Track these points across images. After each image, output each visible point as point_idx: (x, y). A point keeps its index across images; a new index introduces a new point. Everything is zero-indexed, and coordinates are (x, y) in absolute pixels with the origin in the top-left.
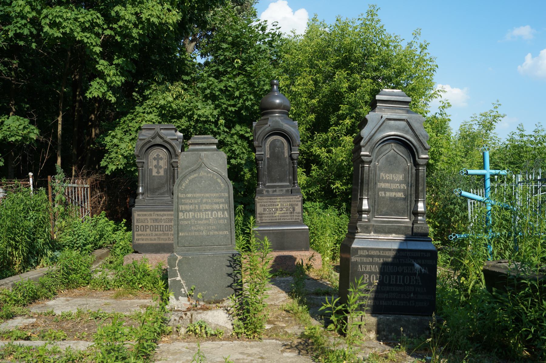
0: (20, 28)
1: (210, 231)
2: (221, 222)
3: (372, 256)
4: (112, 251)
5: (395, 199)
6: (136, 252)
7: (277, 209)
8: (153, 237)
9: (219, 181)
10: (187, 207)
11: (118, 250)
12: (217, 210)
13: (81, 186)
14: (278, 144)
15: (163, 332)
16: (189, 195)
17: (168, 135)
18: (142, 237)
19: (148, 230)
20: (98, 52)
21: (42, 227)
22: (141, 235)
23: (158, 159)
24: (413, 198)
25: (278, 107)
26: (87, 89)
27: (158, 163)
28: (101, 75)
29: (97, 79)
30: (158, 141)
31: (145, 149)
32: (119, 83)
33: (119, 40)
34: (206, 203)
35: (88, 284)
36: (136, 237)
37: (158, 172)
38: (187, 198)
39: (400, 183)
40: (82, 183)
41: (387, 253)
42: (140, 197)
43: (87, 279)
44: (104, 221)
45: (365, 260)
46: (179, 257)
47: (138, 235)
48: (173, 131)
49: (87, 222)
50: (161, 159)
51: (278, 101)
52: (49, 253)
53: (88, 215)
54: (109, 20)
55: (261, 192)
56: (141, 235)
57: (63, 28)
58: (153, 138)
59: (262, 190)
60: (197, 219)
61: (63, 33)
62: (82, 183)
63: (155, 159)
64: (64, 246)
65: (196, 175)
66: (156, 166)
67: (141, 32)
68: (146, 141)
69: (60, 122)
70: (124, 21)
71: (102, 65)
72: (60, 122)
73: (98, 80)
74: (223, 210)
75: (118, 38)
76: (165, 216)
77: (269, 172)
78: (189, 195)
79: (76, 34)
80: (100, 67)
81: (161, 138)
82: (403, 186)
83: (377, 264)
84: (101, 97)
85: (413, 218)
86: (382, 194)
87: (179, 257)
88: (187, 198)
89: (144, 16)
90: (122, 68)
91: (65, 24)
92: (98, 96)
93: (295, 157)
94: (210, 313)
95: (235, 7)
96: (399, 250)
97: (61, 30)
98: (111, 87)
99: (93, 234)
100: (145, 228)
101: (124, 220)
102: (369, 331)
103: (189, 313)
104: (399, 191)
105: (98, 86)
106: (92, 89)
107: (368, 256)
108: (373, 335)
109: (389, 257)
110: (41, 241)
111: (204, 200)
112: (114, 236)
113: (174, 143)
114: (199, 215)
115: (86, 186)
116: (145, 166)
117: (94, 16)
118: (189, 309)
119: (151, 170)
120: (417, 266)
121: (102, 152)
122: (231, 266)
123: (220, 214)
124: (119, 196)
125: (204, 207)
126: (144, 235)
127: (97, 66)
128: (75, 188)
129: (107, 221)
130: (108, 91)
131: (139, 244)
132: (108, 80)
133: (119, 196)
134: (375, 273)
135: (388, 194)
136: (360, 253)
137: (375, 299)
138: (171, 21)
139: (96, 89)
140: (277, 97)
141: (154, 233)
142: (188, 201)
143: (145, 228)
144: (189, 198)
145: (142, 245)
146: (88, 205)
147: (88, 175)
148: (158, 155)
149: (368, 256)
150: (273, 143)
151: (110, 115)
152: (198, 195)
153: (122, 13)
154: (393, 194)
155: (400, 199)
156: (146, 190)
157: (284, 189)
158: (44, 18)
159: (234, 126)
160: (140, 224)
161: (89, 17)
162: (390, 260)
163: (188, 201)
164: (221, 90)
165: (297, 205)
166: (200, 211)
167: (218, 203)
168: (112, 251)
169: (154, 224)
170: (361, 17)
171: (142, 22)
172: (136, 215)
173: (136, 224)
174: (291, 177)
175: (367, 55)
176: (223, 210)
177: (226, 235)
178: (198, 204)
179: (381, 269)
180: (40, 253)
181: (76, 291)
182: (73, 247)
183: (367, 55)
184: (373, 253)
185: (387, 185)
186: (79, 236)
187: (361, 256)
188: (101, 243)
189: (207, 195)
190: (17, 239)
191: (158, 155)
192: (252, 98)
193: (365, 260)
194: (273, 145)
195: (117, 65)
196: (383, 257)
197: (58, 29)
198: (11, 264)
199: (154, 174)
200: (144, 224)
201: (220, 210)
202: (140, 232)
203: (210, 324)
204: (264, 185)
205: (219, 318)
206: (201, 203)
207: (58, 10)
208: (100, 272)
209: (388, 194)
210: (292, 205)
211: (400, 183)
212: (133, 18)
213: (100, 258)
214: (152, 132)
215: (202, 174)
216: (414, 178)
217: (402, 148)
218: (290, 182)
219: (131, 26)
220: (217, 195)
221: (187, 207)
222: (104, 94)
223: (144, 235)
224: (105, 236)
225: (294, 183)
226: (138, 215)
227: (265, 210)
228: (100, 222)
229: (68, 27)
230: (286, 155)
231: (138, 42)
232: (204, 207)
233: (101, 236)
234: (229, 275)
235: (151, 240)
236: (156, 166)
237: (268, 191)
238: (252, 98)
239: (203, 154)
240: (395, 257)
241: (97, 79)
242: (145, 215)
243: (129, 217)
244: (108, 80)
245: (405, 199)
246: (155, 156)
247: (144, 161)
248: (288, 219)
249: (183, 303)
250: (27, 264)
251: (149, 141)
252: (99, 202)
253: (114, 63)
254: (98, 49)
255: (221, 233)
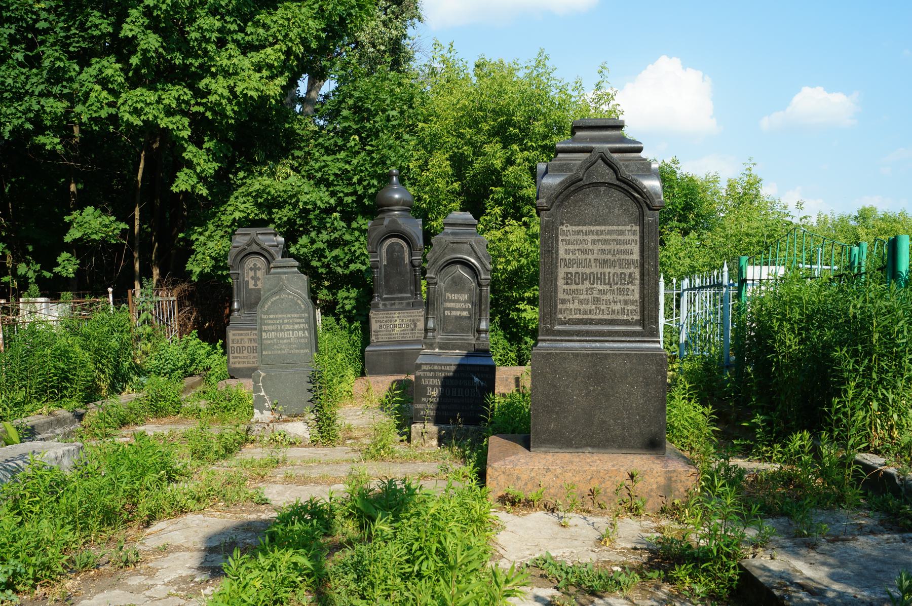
0: (95, 112)
1: (291, 349)
2: (302, 341)
3: (434, 371)
4: (206, 380)
5: (460, 317)
6: (232, 377)
7: (395, 326)
8: (251, 360)
9: (299, 302)
10: (270, 328)
11: (213, 378)
12: (298, 330)
13: (166, 299)
14: (397, 248)
15: (247, 440)
16: (272, 316)
17: (266, 241)
18: (238, 360)
19: (245, 352)
20: (186, 137)
21: (126, 349)
22: (237, 357)
23: (255, 269)
24: (477, 317)
25: (397, 203)
26: (173, 181)
27: (255, 273)
28: (190, 164)
29: (185, 169)
30: (255, 248)
31: (239, 258)
32: (211, 171)
33: (210, 117)
34: (288, 323)
35: (178, 412)
36: (231, 360)
37: (255, 285)
38: (269, 319)
39: (465, 302)
40: (167, 296)
41: (448, 368)
42: (236, 314)
43: (177, 407)
44: (195, 342)
45: (428, 374)
46: (263, 374)
47: (233, 358)
48: (272, 237)
49: (178, 345)
50: (259, 269)
51: (397, 196)
52: (135, 378)
53: (175, 336)
54: (200, 94)
55: (376, 306)
56: (237, 357)
57: (145, 114)
58: (248, 245)
59: (378, 304)
60: (279, 339)
61: (143, 121)
62: (167, 296)
63: (251, 269)
64: (149, 372)
65: (278, 297)
66: (252, 278)
67: (236, 108)
68: (240, 248)
69: (137, 217)
70: (216, 96)
71: (190, 152)
72: (137, 217)
73: (185, 170)
74: (304, 330)
75: (209, 114)
76: (253, 335)
77: (387, 281)
78: (272, 316)
79: (159, 121)
80: (187, 155)
81: (258, 245)
82: (468, 305)
83: (439, 377)
84: (190, 190)
85: (476, 334)
86: (447, 313)
87: (263, 374)
88: (269, 319)
89: (238, 90)
90: (214, 154)
91: (147, 109)
92: (187, 190)
93: (416, 263)
94: (290, 424)
95: (389, 7)
96: (459, 366)
97: (142, 117)
98: (202, 178)
99: (182, 358)
100: (241, 349)
101: (220, 341)
102: (431, 438)
103: (271, 425)
104: (464, 310)
105: (186, 178)
106: (178, 182)
107: (431, 371)
108: (435, 442)
109: (450, 371)
110: (126, 365)
111: (286, 321)
112: (207, 360)
113: (272, 250)
114: (283, 335)
115: (172, 299)
116: (241, 278)
117: (181, 92)
118: (271, 422)
119: (247, 283)
120: (476, 379)
121: (188, 250)
122: (311, 382)
123: (301, 334)
124: (211, 308)
125: (285, 327)
126: (240, 358)
127: (184, 155)
128: (159, 302)
129: (200, 343)
130: (198, 183)
131: (235, 368)
132: (198, 170)
133: (211, 308)
134: (437, 386)
135: (453, 313)
136: (423, 367)
137: (437, 410)
138: (272, 93)
139: (183, 182)
140: (396, 191)
141: (252, 355)
142: (270, 322)
143: (241, 349)
144: (272, 319)
145: (238, 370)
146: (175, 323)
147: (174, 284)
148: (255, 265)
149: (431, 371)
150: (391, 246)
151: (198, 210)
152: (279, 316)
153: (213, 87)
154: (458, 313)
155: (465, 317)
156: (242, 305)
157: (405, 302)
158: (123, 104)
159: (355, 219)
160: (235, 345)
161: (174, 94)
162: (451, 374)
163: (270, 322)
164: (336, 175)
165: (419, 320)
166: (282, 331)
167: (299, 323)
168: (206, 380)
169: (251, 345)
170: (529, 64)
171: (235, 96)
172: (231, 334)
173: (231, 345)
174: (412, 288)
175: (531, 118)
176: (304, 330)
177: (306, 354)
178: (280, 324)
179: (442, 383)
180: (125, 379)
181: (166, 420)
182: (159, 374)
183: (531, 118)
184: (435, 368)
185: (452, 305)
186: (166, 360)
187: (424, 371)
188: (192, 369)
189: (288, 316)
190: (104, 361)
191: (255, 265)
192: (376, 183)
193: (428, 374)
194: (391, 249)
195: (208, 150)
196: (444, 371)
197: (139, 116)
198: (98, 389)
199: (251, 286)
200: (240, 345)
201: (301, 329)
202: (236, 355)
203: (290, 433)
204: (381, 297)
205: (299, 429)
206: (283, 323)
207: (139, 94)
208: (190, 401)
209: (453, 313)
210: (413, 320)
211: (465, 302)
212: (226, 93)
213: (192, 387)
214: (247, 238)
215: (283, 296)
216: (478, 298)
217: (468, 269)
218: (412, 293)
219: (224, 102)
220: (298, 315)
221: (270, 328)
222: (193, 187)
223: (240, 358)
224: (197, 361)
225: (416, 295)
226: (234, 335)
227: (381, 327)
228: (191, 343)
229: (151, 113)
230: (407, 261)
231: (233, 121)
232: (285, 327)
233: (193, 361)
234: (310, 391)
235: (249, 363)
236: (252, 278)
237: (384, 305)
238: (376, 183)
239: (284, 277)
240: (455, 372)
241: (185, 169)
242: (242, 335)
243: (224, 336)
244: (198, 170)
245: (469, 318)
246: (252, 265)
247: (239, 272)
248: (409, 337)
249: (267, 416)
250: (114, 389)
251: (245, 249)
252: (189, 319)
253: (204, 146)
254: (186, 134)
255: (302, 351)
